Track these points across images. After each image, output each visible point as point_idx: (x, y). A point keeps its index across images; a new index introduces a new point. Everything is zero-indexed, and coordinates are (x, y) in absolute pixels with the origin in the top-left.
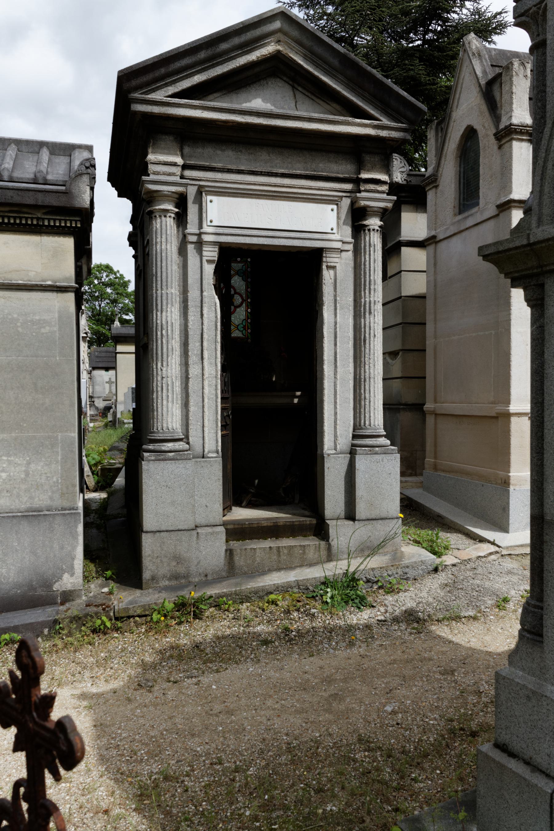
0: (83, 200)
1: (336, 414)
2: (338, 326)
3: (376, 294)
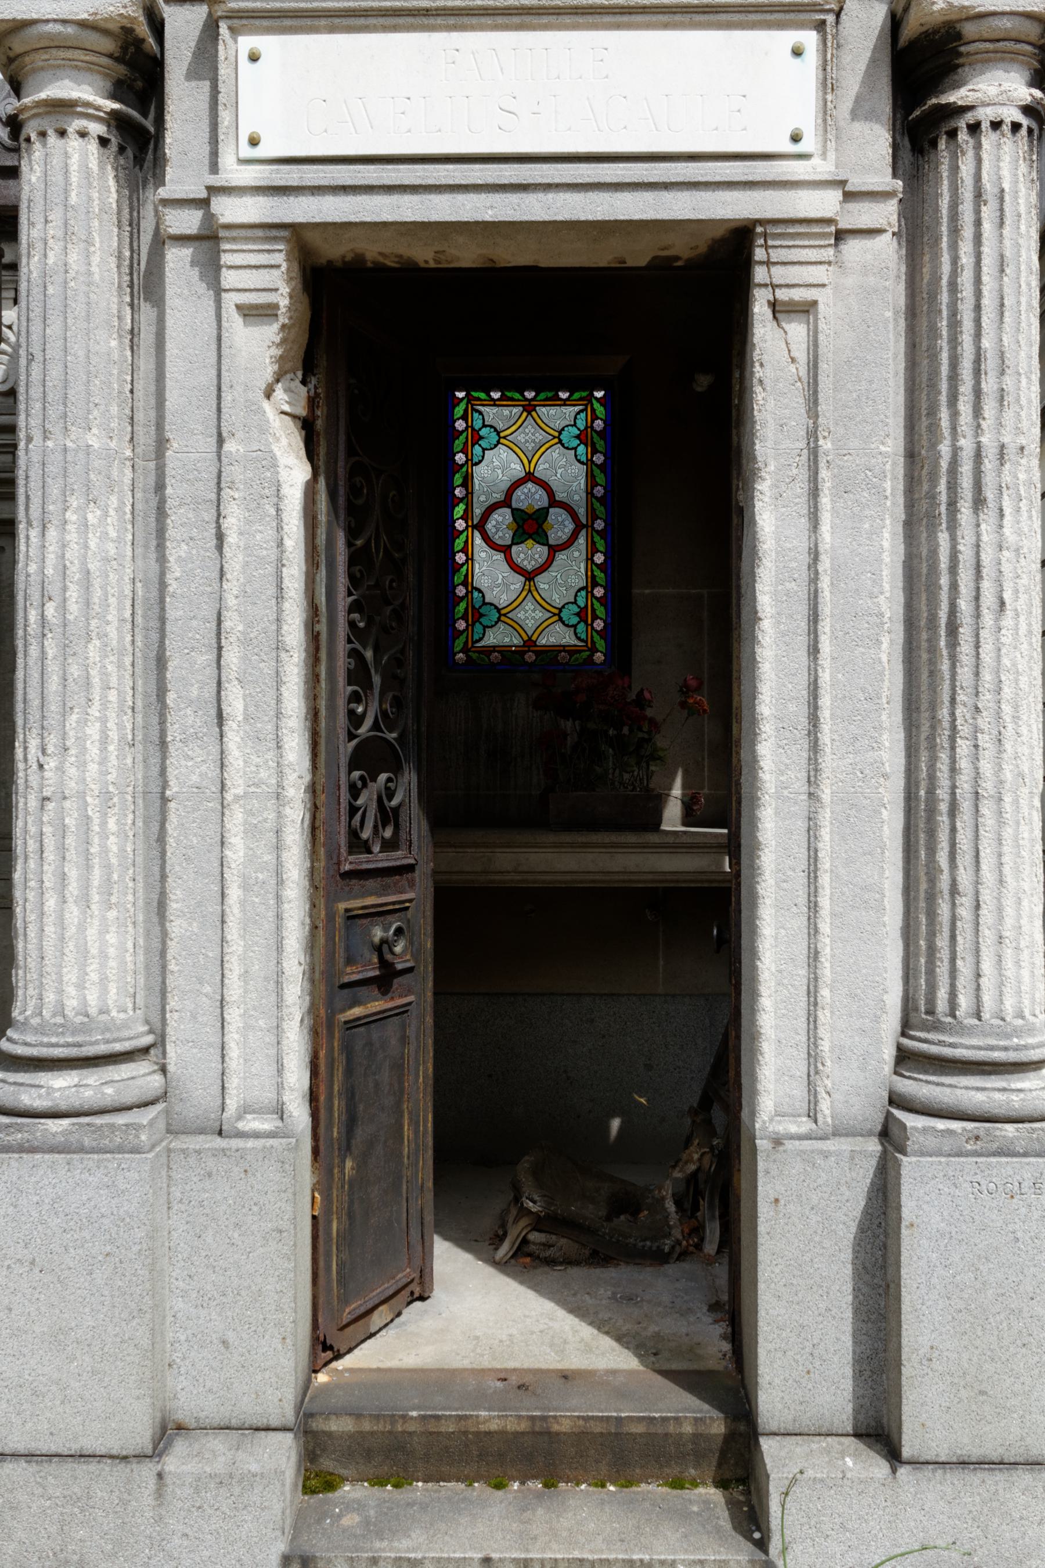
1: (814, 956)
2: (825, 564)
3: (1009, 416)
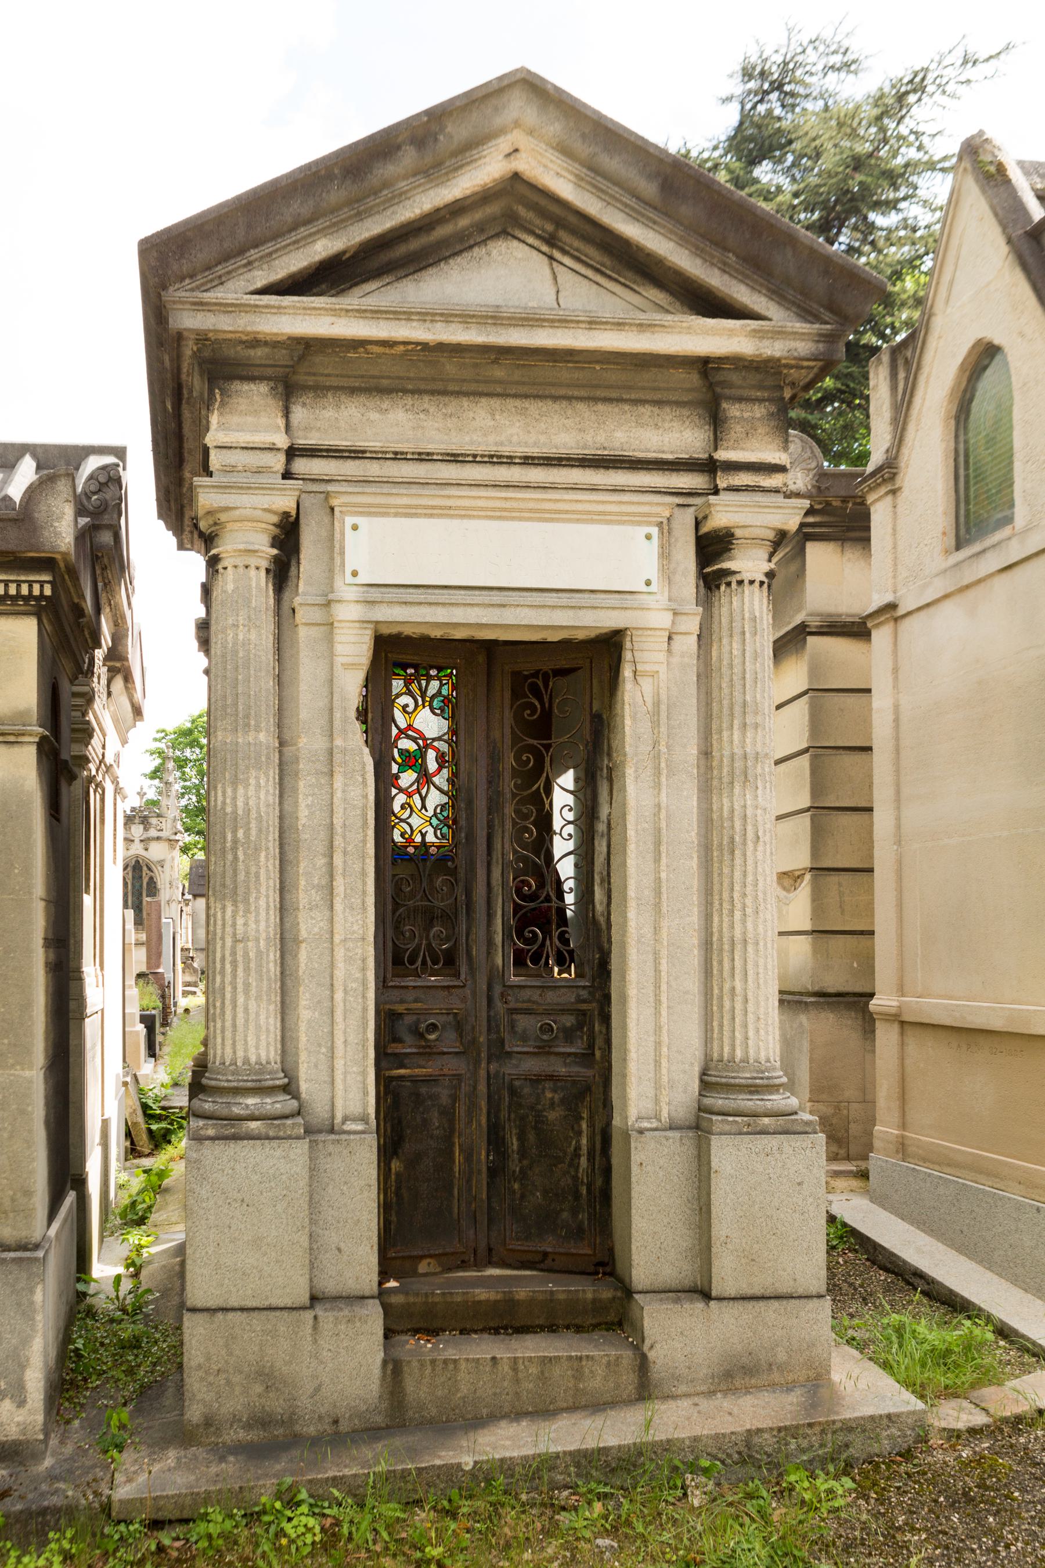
0: (57, 534)
